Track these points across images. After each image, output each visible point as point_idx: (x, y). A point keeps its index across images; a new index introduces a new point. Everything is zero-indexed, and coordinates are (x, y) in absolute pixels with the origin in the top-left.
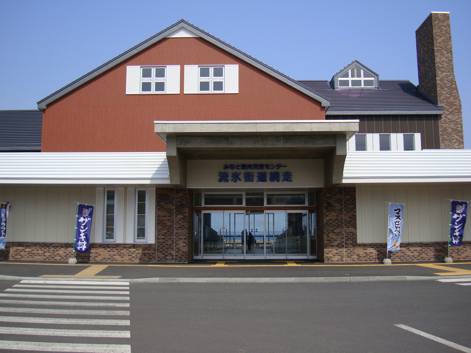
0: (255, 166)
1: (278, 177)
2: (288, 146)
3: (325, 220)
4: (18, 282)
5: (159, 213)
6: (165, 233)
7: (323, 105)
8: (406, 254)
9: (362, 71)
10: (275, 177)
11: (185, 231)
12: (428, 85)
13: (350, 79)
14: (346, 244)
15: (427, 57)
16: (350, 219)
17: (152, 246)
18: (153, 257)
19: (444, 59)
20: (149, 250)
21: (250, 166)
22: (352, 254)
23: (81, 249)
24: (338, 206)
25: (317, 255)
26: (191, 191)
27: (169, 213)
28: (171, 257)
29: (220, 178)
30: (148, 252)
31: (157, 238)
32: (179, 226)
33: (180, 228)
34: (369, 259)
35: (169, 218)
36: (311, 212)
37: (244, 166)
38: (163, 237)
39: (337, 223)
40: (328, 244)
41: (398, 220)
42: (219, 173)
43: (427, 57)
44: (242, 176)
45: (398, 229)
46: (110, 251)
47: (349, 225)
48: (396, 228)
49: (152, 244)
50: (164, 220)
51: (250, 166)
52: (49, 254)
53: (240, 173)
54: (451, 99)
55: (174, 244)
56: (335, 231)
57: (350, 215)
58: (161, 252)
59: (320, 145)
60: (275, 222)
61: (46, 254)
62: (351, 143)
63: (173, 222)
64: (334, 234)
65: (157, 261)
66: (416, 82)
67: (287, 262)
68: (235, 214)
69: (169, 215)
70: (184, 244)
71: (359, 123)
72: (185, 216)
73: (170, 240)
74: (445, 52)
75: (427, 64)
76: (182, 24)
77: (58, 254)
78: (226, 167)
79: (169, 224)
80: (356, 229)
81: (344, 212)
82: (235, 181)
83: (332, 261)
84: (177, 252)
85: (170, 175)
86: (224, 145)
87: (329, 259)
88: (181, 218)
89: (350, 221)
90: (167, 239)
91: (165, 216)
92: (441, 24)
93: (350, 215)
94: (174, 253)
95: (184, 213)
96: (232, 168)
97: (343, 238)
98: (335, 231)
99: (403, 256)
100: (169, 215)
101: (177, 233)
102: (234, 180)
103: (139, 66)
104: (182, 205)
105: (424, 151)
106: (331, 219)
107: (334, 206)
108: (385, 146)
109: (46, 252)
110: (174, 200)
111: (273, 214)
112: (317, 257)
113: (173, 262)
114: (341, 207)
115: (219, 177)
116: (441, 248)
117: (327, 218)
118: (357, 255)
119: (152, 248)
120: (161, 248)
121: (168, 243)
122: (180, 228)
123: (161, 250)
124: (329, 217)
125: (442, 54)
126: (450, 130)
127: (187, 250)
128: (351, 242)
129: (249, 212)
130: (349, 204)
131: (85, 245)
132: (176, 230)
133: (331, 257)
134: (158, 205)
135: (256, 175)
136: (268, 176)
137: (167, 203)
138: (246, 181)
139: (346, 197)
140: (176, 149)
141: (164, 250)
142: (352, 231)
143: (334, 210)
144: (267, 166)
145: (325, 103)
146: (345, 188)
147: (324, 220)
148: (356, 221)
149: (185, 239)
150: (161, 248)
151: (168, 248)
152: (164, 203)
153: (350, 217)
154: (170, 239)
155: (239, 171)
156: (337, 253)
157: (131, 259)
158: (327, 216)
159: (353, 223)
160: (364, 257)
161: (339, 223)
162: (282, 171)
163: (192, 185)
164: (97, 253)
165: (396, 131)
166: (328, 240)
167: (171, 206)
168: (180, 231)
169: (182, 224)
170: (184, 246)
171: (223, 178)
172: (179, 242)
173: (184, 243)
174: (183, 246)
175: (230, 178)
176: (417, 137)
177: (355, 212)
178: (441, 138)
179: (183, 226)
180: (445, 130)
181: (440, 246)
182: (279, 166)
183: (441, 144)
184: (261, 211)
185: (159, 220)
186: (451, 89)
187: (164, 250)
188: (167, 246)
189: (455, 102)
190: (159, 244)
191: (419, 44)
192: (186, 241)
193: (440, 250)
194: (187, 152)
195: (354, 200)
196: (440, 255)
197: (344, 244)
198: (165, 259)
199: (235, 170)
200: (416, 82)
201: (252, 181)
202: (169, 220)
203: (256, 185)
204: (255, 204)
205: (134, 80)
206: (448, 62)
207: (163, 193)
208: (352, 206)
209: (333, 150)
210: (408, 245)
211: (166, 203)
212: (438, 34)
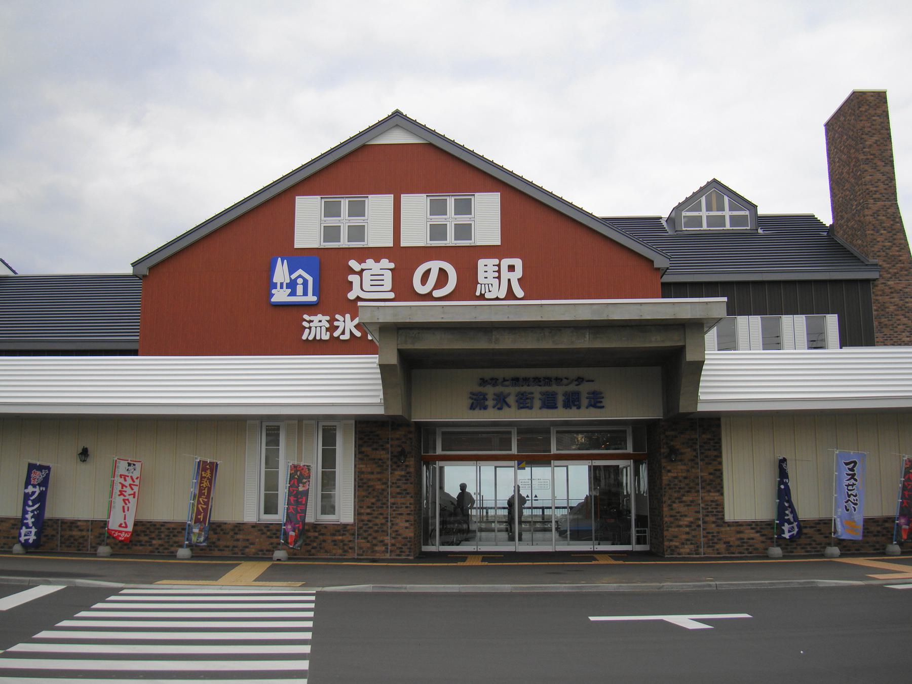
0: (537, 380)
1: (578, 399)
2: (598, 344)
3: (666, 478)
4: (116, 591)
5: (361, 466)
6: (373, 504)
7: (656, 266)
8: (814, 541)
9: (726, 199)
10: (572, 401)
11: (409, 500)
12: (850, 224)
13: (704, 213)
14: (704, 522)
15: (848, 173)
16: (711, 477)
17: (349, 527)
18: (351, 548)
19: (879, 176)
20: (343, 535)
21: (526, 380)
22: (716, 540)
23: (26, 541)
24: (688, 453)
25: (651, 544)
26: (418, 424)
27: (379, 466)
28: (383, 548)
29: (472, 404)
30: (340, 538)
31: (358, 514)
32: (398, 490)
33: (399, 493)
34: (747, 549)
35: (379, 476)
36: (637, 463)
37: (516, 381)
38: (368, 511)
39: (687, 484)
40: (671, 523)
41: (852, 481)
42: (471, 393)
43: (848, 173)
44: (511, 400)
45: (852, 498)
46: (271, 537)
47: (708, 488)
48: (849, 496)
49: (348, 525)
50: (369, 480)
51: (526, 380)
52: (160, 542)
53: (509, 394)
54: (894, 251)
55: (389, 524)
56: (684, 498)
57: (711, 468)
58: (365, 538)
59: (656, 341)
60: (565, 484)
61: (154, 542)
62: (711, 337)
63: (386, 483)
64: (682, 505)
65: (358, 555)
66: (827, 219)
67: (596, 556)
68: (496, 467)
69: (378, 470)
70: (407, 524)
71: (727, 303)
72: (408, 473)
73: (381, 517)
74: (879, 163)
75: (847, 186)
76: (397, 120)
77: (175, 542)
78: (483, 382)
79: (379, 486)
80: (722, 494)
81: (700, 463)
82: (500, 409)
83: (679, 554)
84: (394, 538)
85: (385, 399)
86: (482, 344)
87: (673, 550)
88: (401, 476)
89: (711, 480)
90: (375, 513)
91: (373, 473)
92: (872, 111)
93: (711, 468)
94: (388, 540)
95: (407, 466)
96: (494, 385)
97: (699, 512)
98: (684, 498)
99: (810, 544)
100: (378, 470)
101: (394, 504)
102: (499, 406)
103: (319, 197)
104: (403, 453)
105: (846, 350)
106: (675, 478)
107: (682, 454)
108: (772, 341)
109: (153, 539)
110: (388, 443)
111: (567, 467)
112: (651, 547)
113: (388, 556)
114: (694, 454)
115: (470, 401)
116: (879, 529)
117: (670, 474)
118: (725, 543)
119: (347, 531)
120: (365, 531)
121: (378, 521)
122: (399, 493)
123: (365, 535)
124: (673, 472)
125: (875, 167)
126: (892, 308)
127: (412, 535)
128: (713, 519)
129: (523, 464)
130: (709, 450)
131: (33, 533)
132: (392, 497)
133: (676, 547)
134: (361, 453)
135: (537, 396)
136: (560, 399)
137: (376, 449)
138: (520, 408)
139: (704, 436)
140: (396, 351)
141: (370, 535)
142: (716, 498)
143: (681, 460)
144: (558, 380)
145: (660, 262)
146: (702, 419)
147: (664, 478)
148: (722, 480)
149: (409, 514)
150: (365, 531)
151: (377, 531)
152: (370, 449)
153: (710, 474)
154: (381, 514)
155: (506, 390)
156: (687, 540)
157: (310, 551)
158: (669, 471)
159: (716, 483)
160: (739, 546)
161: (692, 485)
162: (585, 389)
163: (421, 416)
164: (248, 540)
165: (793, 311)
166: (671, 516)
167: (382, 454)
168: (399, 500)
169: (404, 487)
170: (406, 528)
171: (478, 402)
172: (398, 521)
173: (407, 521)
174: (405, 527)
175: (490, 403)
176: (832, 321)
177: (721, 463)
178: (875, 324)
179: (406, 490)
180: (883, 307)
181: (878, 526)
182: (580, 380)
183: (876, 335)
184: (545, 460)
185: (361, 480)
186: (894, 232)
187: (370, 535)
188: (376, 528)
189: (900, 256)
190: (361, 524)
191: (832, 148)
192: (411, 518)
193: (878, 532)
194: (416, 359)
195: (719, 442)
196: (878, 542)
197: (701, 522)
198: (373, 552)
199: (499, 389)
200: (827, 219)
201: (531, 408)
202: (379, 480)
203: (536, 415)
204: (534, 449)
205: (310, 222)
206: (887, 182)
207: (367, 429)
208: (716, 453)
209: (680, 351)
210: (819, 524)
211: (373, 449)
212: (866, 130)
